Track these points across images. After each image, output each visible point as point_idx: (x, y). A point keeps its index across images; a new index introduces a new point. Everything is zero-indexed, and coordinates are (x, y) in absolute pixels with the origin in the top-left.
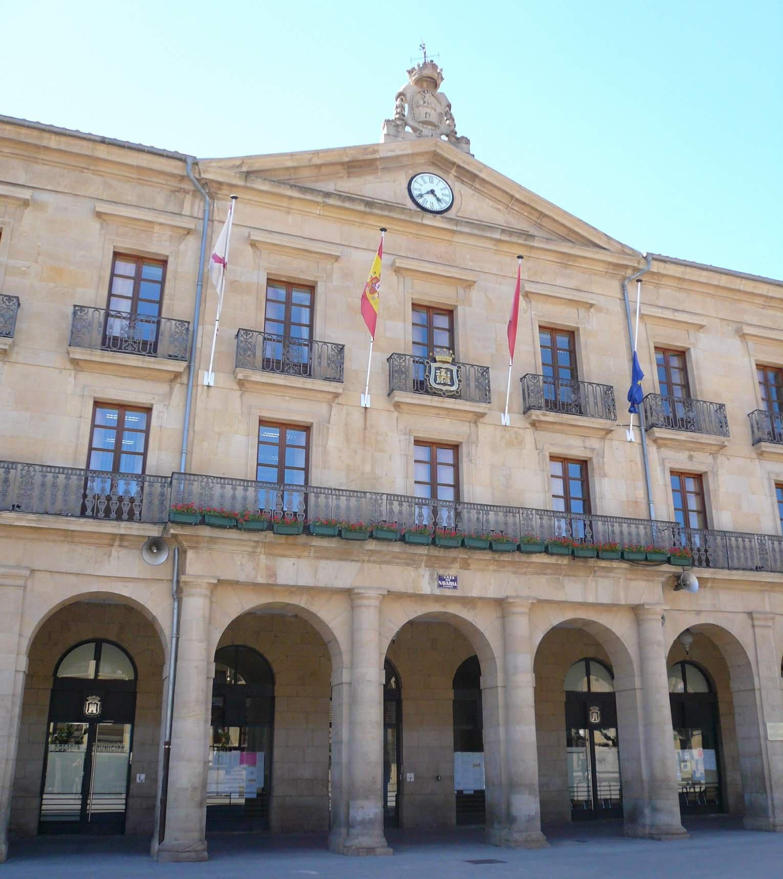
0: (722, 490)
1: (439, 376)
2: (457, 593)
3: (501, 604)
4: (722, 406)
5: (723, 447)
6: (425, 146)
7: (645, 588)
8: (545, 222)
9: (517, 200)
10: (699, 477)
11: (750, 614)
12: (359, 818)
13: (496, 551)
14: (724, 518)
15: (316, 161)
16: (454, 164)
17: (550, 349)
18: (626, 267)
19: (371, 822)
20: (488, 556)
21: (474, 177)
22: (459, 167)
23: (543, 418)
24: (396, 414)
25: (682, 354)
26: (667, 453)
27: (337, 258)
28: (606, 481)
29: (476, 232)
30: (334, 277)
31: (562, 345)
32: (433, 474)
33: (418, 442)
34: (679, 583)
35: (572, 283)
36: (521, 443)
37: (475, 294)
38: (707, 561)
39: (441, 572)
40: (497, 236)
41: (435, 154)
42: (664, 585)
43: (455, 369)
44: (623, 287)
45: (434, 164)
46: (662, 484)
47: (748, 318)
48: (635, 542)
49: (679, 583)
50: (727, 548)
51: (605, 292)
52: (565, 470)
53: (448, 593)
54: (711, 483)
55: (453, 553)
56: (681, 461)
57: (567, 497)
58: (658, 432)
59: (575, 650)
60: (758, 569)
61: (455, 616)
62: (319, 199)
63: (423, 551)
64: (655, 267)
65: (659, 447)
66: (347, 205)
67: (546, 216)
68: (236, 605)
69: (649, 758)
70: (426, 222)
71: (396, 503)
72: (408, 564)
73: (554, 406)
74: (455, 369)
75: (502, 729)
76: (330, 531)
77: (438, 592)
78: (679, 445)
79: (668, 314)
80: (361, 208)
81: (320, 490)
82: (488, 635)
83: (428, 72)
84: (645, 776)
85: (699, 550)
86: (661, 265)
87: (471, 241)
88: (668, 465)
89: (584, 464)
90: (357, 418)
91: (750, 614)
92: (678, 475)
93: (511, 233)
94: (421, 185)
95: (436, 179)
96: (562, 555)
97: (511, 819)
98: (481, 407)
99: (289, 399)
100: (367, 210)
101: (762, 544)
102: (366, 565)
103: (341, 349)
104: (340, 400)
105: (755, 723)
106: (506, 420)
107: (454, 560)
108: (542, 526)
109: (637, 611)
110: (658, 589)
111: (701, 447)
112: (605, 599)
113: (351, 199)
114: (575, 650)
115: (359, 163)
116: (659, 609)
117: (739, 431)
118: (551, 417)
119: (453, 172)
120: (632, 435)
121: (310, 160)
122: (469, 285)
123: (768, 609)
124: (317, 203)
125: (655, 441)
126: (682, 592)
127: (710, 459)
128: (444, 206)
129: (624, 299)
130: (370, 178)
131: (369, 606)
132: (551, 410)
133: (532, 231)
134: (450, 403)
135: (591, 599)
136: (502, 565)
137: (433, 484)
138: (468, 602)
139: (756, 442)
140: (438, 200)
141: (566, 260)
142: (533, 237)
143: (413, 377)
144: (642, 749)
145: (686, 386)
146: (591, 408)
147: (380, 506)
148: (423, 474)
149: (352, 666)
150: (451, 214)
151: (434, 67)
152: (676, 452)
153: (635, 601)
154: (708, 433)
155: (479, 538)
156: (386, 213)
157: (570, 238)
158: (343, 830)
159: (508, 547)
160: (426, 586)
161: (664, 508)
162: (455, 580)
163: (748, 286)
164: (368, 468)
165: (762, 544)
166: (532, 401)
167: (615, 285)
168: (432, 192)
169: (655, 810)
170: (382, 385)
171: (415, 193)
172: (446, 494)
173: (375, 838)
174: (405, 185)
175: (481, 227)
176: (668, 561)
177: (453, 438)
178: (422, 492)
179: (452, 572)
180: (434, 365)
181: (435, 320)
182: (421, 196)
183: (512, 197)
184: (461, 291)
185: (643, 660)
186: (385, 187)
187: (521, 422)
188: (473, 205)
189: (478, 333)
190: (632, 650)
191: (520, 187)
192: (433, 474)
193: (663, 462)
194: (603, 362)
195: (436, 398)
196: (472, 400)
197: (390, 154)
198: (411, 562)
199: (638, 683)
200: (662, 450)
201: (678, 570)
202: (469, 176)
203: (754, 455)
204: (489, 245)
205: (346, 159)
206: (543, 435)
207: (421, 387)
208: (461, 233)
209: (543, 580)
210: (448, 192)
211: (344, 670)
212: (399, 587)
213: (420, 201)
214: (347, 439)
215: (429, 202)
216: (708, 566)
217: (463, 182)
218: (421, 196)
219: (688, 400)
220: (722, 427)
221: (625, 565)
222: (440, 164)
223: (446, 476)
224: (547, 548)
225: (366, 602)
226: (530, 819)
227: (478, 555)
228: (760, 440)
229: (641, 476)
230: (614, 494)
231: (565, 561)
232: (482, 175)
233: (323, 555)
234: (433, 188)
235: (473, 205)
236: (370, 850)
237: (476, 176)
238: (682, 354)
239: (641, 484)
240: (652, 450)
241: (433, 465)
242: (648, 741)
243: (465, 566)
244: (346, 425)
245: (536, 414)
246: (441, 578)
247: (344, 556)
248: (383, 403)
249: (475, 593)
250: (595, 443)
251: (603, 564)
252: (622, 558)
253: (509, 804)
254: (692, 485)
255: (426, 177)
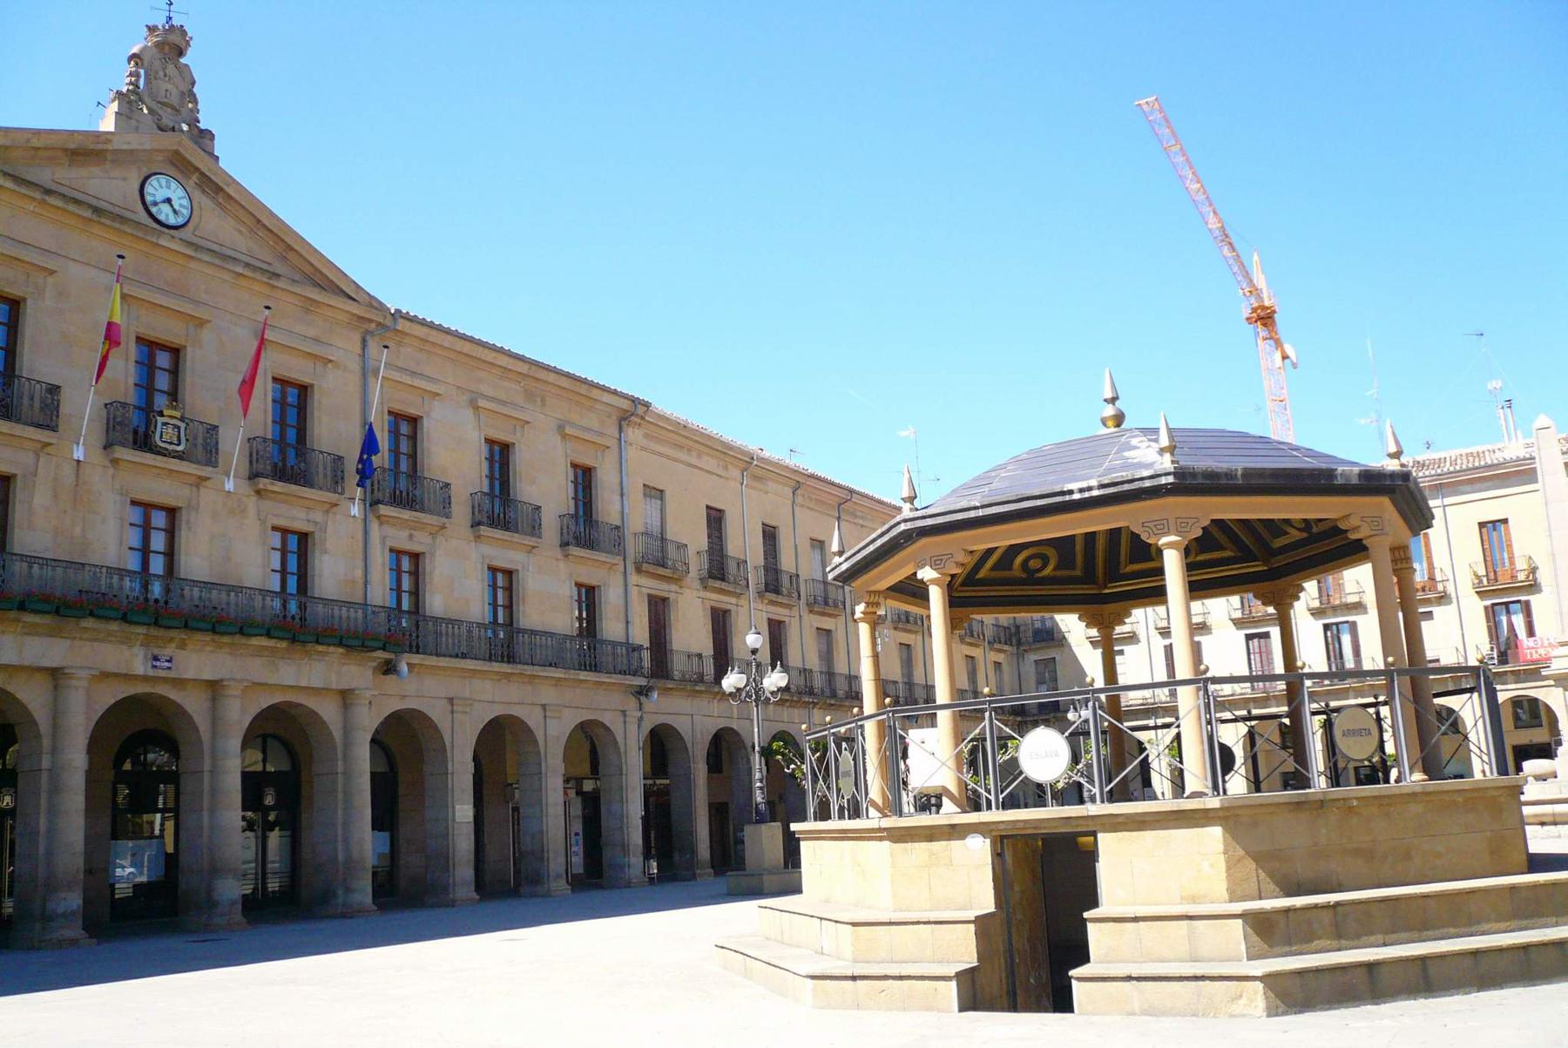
0: (437, 572)
1: (163, 434)
2: (172, 674)
3: (214, 687)
4: (447, 485)
5: (443, 527)
6: (167, 141)
7: (356, 673)
8: (291, 255)
9: (264, 226)
10: (416, 557)
11: (451, 700)
12: (61, 910)
13: (131, 623)
14: (436, 603)
15: (35, 143)
16: (197, 169)
17: (280, 403)
18: (370, 321)
19: (73, 913)
20: (208, 637)
21: (219, 189)
22: (203, 174)
23: (270, 488)
24: (111, 471)
25: (414, 421)
26: (389, 530)
27: (52, 272)
28: (326, 558)
29: (217, 261)
30: (47, 295)
31: (295, 401)
32: (146, 539)
33: (134, 503)
34: (389, 669)
35: (312, 332)
36: (244, 511)
37: (206, 334)
38: (418, 646)
39: (156, 651)
40: (240, 270)
41: (177, 152)
42: (375, 669)
43: (183, 426)
44: (364, 341)
45: (172, 164)
46: (380, 562)
47: (485, 389)
48: (345, 626)
49: (389, 669)
50: (438, 634)
51: (345, 347)
52: (284, 542)
53: (162, 673)
54: (427, 565)
55: (173, 633)
56: (401, 540)
57: (284, 572)
58: (384, 510)
59: (284, 735)
60: (464, 656)
61: (162, 697)
62: (38, 195)
63: (141, 630)
64: (402, 325)
65: (381, 524)
66: (71, 207)
67: (292, 249)
68: (109, 696)
69: (346, 840)
70: (163, 242)
71: (116, 578)
72: (122, 643)
73: (281, 474)
74: (183, 426)
75: (205, 814)
76: (47, 607)
77: (151, 672)
78: (403, 524)
79: (407, 379)
80: (88, 213)
81: (520, 631)
82: (197, 719)
83: (175, 38)
84: (341, 857)
85: (156, 601)
86: (408, 324)
87: (208, 270)
88: (389, 543)
89: (304, 537)
90: (68, 470)
91: (451, 700)
92: (397, 553)
93: (255, 268)
94: (158, 189)
95: (174, 184)
96: (282, 639)
97: (212, 904)
98: (206, 471)
99: (158, 481)
100: (95, 217)
101: (470, 631)
102: (77, 643)
103: (54, 390)
104: (49, 449)
105: (445, 805)
106: (230, 485)
107: (171, 640)
108: (263, 607)
109: (346, 697)
110: (370, 672)
111: (421, 526)
112: (317, 684)
113: (76, 202)
114: (284, 735)
115: (84, 150)
116: (368, 694)
117: (461, 511)
118: (279, 486)
119: (195, 178)
120: (356, 510)
121: (28, 140)
122: (201, 323)
123: (467, 694)
124: (34, 199)
125: (379, 517)
126: (392, 678)
127: (429, 540)
128: (181, 221)
129: (363, 356)
130: (95, 170)
131: (77, 688)
132: (280, 479)
133: (278, 267)
134: (174, 464)
135: (304, 683)
136: (220, 646)
137: (145, 551)
138: (179, 683)
139: (476, 524)
140: (175, 212)
141: (309, 305)
142: (278, 276)
143: (133, 430)
144: (340, 832)
145: (413, 457)
146: (320, 479)
147: (99, 579)
148: (134, 538)
149: (54, 751)
150: (184, 234)
151: (184, 33)
152: (400, 529)
153: (344, 686)
154: (431, 512)
155: (203, 618)
156: (117, 225)
157: (322, 280)
158: (38, 926)
159: (176, 623)
160: (139, 666)
161: (380, 592)
162: (169, 661)
163: (490, 356)
164: (78, 530)
165: (470, 631)
166: (260, 467)
167: (357, 337)
168: (168, 201)
169: (348, 890)
170: (98, 439)
171: (149, 199)
172: (157, 565)
173: (75, 931)
174: (137, 186)
175: (224, 258)
176: (384, 649)
177: (172, 502)
178: (133, 563)
179: (169, 650)
180: (160, 420)
181: (161, 363)
182: (155, 204)
183: (259, 221)
184: (192, 329)
185: (347, 744)
186: (113, 187)
187: (246, 489)
188: (217, 226)
189: (210, 387)
190: (337, 735)
191: (271, 213)
192: (146, 539)
193: (384, 539)
194: (334, 430)
195: (159, 458)
196: (198, 463)
197: (125, 147)
198: (127, 641)
199: (207, 766)
200: (385, 526)
201: (392, 656)
202: (214, 187)
203: (560, 556)
204: (227, 276)
205: (72, 146)
206: (267, 505)
207: (143, 442)
208: (199, 260)
209: (258, 661)
210: (185, 202)
211: (1322, 768)
212: (111, 667)
213: (154, 210)
214: (56, 496)
215: (164, 213)
216: (418, 652)
217: (204, 192)
218: (155, 204)
219: (414, 474)
220: (445, 507)
221: (341, 650)
222: (180, 166)
223: (158, 542)
224: (125, 615)
225: (74, 682)
226: (233, 903)
227: (199, 636)
228: (479, 524)
229: (360, 556)
230: (334, 573)
231: (284, 644)
232: (230, 191)
233: (32, 631)
234: (168, 194)
235: (217, 226)
236: (74, 942)
237: (222, 190)
238: (414, 421)
239: (360, 564)
240: (374, 525)
241: (146, 529)
242: (346, 825)
243: (182, 646)
244: (55, 479)
245: (264, 483)
246: (156, 658)
247: (53, 633)
248: (98, 457)
249: (190, 675)
250: (318, 516)
251: (320, 648)
252: (340, 644)
253: (210, 890)
254: (408, 567)
255: (163, 179)
